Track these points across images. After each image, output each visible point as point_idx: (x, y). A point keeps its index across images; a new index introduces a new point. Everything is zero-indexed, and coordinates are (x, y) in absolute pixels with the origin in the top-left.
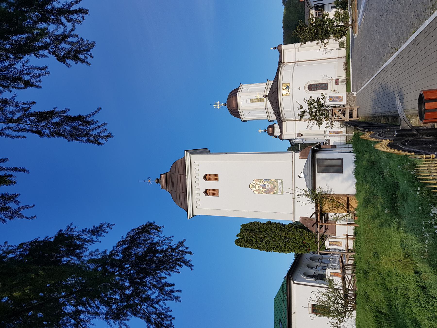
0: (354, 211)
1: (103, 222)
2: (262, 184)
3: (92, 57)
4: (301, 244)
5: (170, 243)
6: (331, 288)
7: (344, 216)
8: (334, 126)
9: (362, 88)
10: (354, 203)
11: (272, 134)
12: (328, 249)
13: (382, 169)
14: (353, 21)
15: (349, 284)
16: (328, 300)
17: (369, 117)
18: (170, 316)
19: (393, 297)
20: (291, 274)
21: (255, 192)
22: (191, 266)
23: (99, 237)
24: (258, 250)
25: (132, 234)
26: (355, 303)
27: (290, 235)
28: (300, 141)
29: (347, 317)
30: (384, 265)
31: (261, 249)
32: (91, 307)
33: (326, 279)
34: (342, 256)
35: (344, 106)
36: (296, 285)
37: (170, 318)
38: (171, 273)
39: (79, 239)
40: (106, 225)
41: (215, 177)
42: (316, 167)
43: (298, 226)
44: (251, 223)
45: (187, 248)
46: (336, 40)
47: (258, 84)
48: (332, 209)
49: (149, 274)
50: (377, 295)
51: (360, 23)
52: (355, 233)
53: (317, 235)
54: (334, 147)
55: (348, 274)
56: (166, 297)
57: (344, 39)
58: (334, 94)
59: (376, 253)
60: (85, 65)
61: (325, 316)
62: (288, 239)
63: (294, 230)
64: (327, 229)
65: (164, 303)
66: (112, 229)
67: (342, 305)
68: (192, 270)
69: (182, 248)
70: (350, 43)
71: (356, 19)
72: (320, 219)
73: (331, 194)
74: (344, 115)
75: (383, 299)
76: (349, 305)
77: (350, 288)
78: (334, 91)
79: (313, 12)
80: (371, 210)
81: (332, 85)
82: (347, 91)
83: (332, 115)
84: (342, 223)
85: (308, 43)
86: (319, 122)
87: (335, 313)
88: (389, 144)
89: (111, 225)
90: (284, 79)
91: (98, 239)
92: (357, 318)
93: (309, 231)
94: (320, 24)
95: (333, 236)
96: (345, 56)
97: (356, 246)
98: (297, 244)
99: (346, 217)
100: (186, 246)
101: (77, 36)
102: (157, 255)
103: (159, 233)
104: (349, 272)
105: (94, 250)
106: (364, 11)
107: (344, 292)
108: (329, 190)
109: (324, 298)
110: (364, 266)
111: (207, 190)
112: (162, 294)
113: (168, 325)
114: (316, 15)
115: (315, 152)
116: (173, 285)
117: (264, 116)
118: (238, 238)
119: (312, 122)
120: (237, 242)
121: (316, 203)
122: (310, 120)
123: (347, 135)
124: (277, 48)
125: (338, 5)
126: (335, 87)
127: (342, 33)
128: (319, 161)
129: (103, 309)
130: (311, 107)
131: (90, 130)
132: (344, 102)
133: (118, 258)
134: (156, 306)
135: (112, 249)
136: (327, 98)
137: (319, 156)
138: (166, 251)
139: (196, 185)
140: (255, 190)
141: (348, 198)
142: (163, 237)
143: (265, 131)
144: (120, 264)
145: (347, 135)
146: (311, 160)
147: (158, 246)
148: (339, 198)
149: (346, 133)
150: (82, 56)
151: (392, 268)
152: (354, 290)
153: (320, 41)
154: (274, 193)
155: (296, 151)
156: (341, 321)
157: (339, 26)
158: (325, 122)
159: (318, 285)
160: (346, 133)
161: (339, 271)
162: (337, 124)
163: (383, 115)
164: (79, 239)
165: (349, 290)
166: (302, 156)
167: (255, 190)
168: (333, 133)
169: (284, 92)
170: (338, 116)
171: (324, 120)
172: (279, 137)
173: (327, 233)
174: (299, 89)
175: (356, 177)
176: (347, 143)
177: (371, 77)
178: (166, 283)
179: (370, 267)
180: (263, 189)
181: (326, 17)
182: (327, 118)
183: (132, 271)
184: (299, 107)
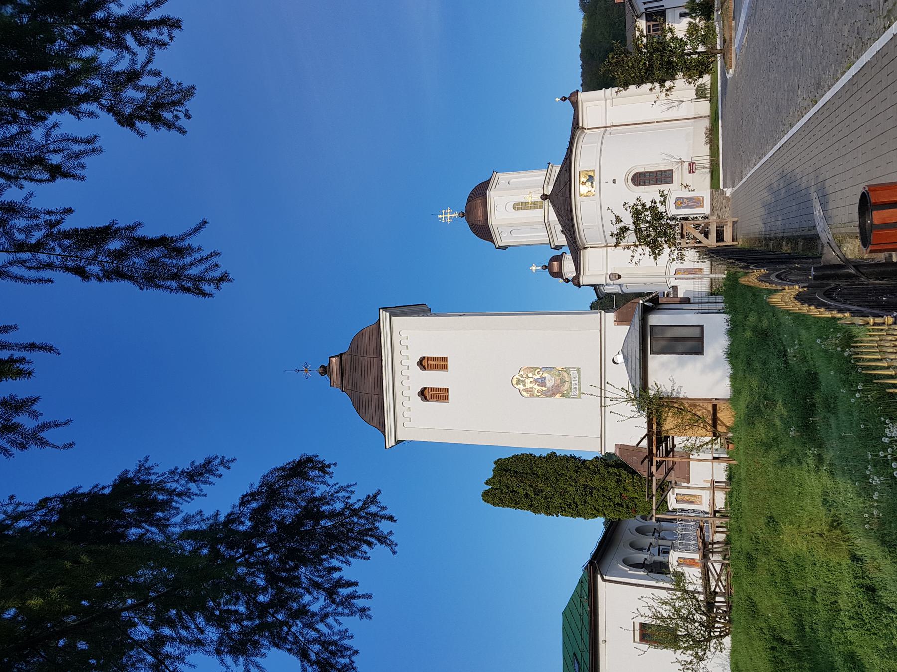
0: (726, 433)
1: (212, 455)
2: (538, 376)
3: (188, 116)
4: (618, 500)
5: (349, 498)
6: (679, 591)
7: (707, 443)
8: (685, 258)
9: (744, 180)
10: (726, 416)
11: (559, 274)
12: (674, 510)
13: (784, 347)
14: (725, 42)
15: (717, 581)
16: (673, 614)
17: (757, 239)
18: (348, 648)
19: (807, 609)
20: (598, 562)
21: (524, 394)
22: (391, 545)
23: (202, 486)
24: (529, 513)
25: (272, 479)
26: (730, 621)
27: (595, 482)
28: (617, 290)
29: (712, 650)
30: (789, 543)
31: (536, 510)
32: (187, 628)
33: (669, 573)
34: (701, 524)
35: (706, 217)
36: (608, 584)
37: (349, 652)
38: (350, 559)
39: (163, 490)
40: (218, 461)
41: (442, 363)
42: (650, 342)
43: (611, 462)
44: (516, 457)
45: (384, 508)
46: (690, 83)
47: (530, 173)
48: (681, 428)
49: (305, 561)
50: (773, 605)
51: (740, 48)
52: (730, 478)
53: (650, 481)
54: (686, 301)
55: (715, 562)
56: (340, 609)
57: (706, 79)
58: (686, 194)
59: (771, 517)
60: (174, 132)
61: (666, 647)
62: (591, 489)
63: (602, 470)
64: (672, 468)
65: (337, 621)
66: (229, 468)
67: (701, 624)
68: (394, 552)
69: (373, 509)
70: (719, 89)
71: (731, 39)
72: (658, 449)
73: (679, 398)
74: (706, 236)
75: (786, 612)
76: (716, 625)
77: (717, 590)
78: (686, 186)
79: (642, 24)
80: (761, 431)
81: (681, 175)
82: (711, 187)
83: (682, 237)
84: (702, 456)
85: (632, 88)
86: (656, 249)
87: (687, 641)
88: (797, 295)
89: (228, 461)
90: (583, 161)
91: (201, 490)
92: (734, 651)
93: (634, 473)
94: (658, 50)
95: (683, 484)
96: (708, 114)
97: (731, 503)
98: (610, 499)
99: (709, 446)
100: (382, 505)
101: (157, 73)
102: (323, 522)
103: (327, 477)
104: (716, 557)
105: (193, 513)
106: (747, 23)
107: (706, 597)
108: (676, 388)
109: (666, 611)
110: (747, 545)
111: (425, 388)
112: (333, 601)
113: (345, 665)
114: (649, 31)
115: (646, 311)
116: (356, 584)
117: (541, 237)
118: (488, 487)
119: (640, 249)
120: (486, 496)
121: (649, 417)
122: (637, 246)
123: (713, 276)
124: (569, 98)
125: (693, 10)
126: (689, 178)
127: (702, 67)
128: (656, 329)
129: (212, 634)
130: (638, 219)
131: (184, 267)
132: (706, 209)
133: (241, 528)
134: (321, 626)
135: (229, 511)
136: (671, 201)
137: (655, 319)
138: (341, 513)
139: (402, 379)
140: (524, 390)
141: (714, 406)
142: (335, 485)
143: (545, 267)
144: (245, 541)
145: (713, 276)
146: (637, 328)
147: (324, 504)
148: (695, 406)
149: (711, 273)
150: (168, 116)
151: (805, 549)
152: (727, 594)
153: (657, 85)
154: (563, 396)
155: (607, 309)
156: (701, 659)
157: (696, 53)
158: (667, 250)
159: (653, 583)
160: (711, 273)
161: (697, 556)
162: (691, 255)
163: (785, 235)
164: (163, 490)
165: (716, 593)
166: (621, 321)
167: (524, 390)
168: (683, 273)
169: (583, 189)
170: (695, 239)
171: (665, 246)
172: (572, 280)
173: (672, 478)
174: (614, 181)
175: (730, 362)
176: (711, 294)
177: (761, 159)
178: (340, 579)
179: (760, 547)
180: (539, 388)
181: (669, 35)
182: (671, 242)
183: (271, 556)
184: (614, 220)
